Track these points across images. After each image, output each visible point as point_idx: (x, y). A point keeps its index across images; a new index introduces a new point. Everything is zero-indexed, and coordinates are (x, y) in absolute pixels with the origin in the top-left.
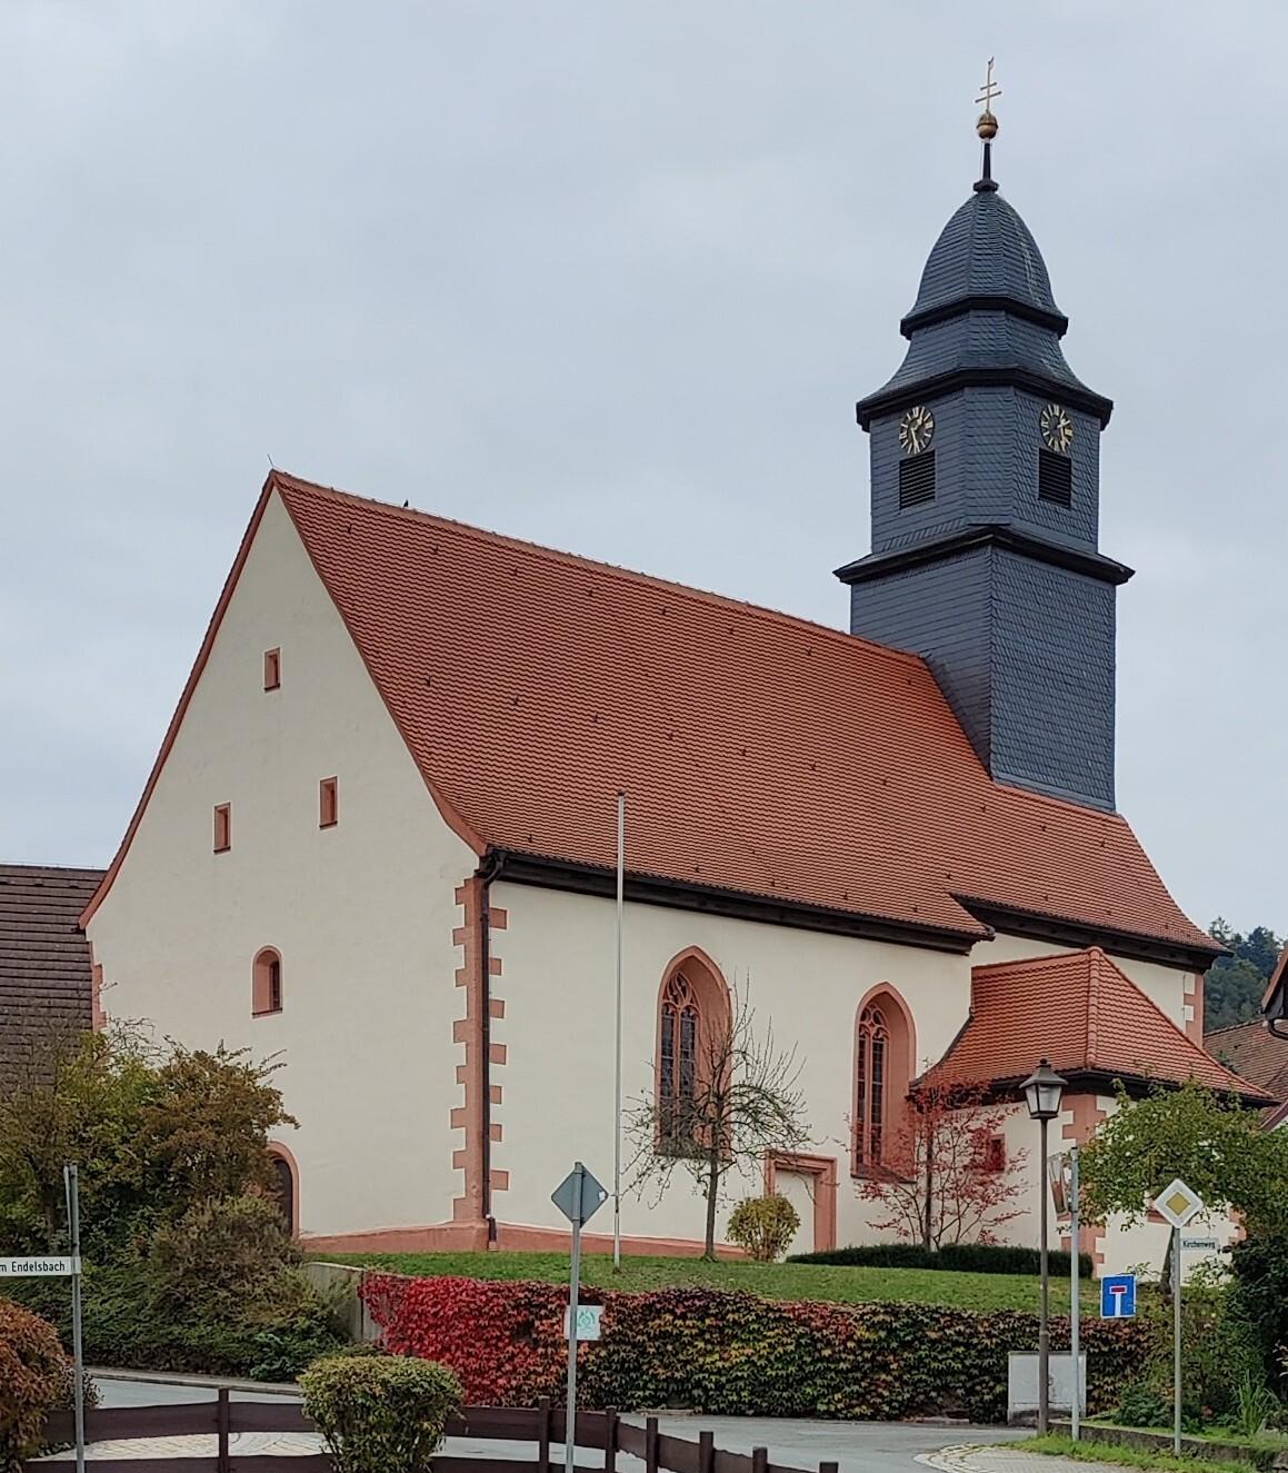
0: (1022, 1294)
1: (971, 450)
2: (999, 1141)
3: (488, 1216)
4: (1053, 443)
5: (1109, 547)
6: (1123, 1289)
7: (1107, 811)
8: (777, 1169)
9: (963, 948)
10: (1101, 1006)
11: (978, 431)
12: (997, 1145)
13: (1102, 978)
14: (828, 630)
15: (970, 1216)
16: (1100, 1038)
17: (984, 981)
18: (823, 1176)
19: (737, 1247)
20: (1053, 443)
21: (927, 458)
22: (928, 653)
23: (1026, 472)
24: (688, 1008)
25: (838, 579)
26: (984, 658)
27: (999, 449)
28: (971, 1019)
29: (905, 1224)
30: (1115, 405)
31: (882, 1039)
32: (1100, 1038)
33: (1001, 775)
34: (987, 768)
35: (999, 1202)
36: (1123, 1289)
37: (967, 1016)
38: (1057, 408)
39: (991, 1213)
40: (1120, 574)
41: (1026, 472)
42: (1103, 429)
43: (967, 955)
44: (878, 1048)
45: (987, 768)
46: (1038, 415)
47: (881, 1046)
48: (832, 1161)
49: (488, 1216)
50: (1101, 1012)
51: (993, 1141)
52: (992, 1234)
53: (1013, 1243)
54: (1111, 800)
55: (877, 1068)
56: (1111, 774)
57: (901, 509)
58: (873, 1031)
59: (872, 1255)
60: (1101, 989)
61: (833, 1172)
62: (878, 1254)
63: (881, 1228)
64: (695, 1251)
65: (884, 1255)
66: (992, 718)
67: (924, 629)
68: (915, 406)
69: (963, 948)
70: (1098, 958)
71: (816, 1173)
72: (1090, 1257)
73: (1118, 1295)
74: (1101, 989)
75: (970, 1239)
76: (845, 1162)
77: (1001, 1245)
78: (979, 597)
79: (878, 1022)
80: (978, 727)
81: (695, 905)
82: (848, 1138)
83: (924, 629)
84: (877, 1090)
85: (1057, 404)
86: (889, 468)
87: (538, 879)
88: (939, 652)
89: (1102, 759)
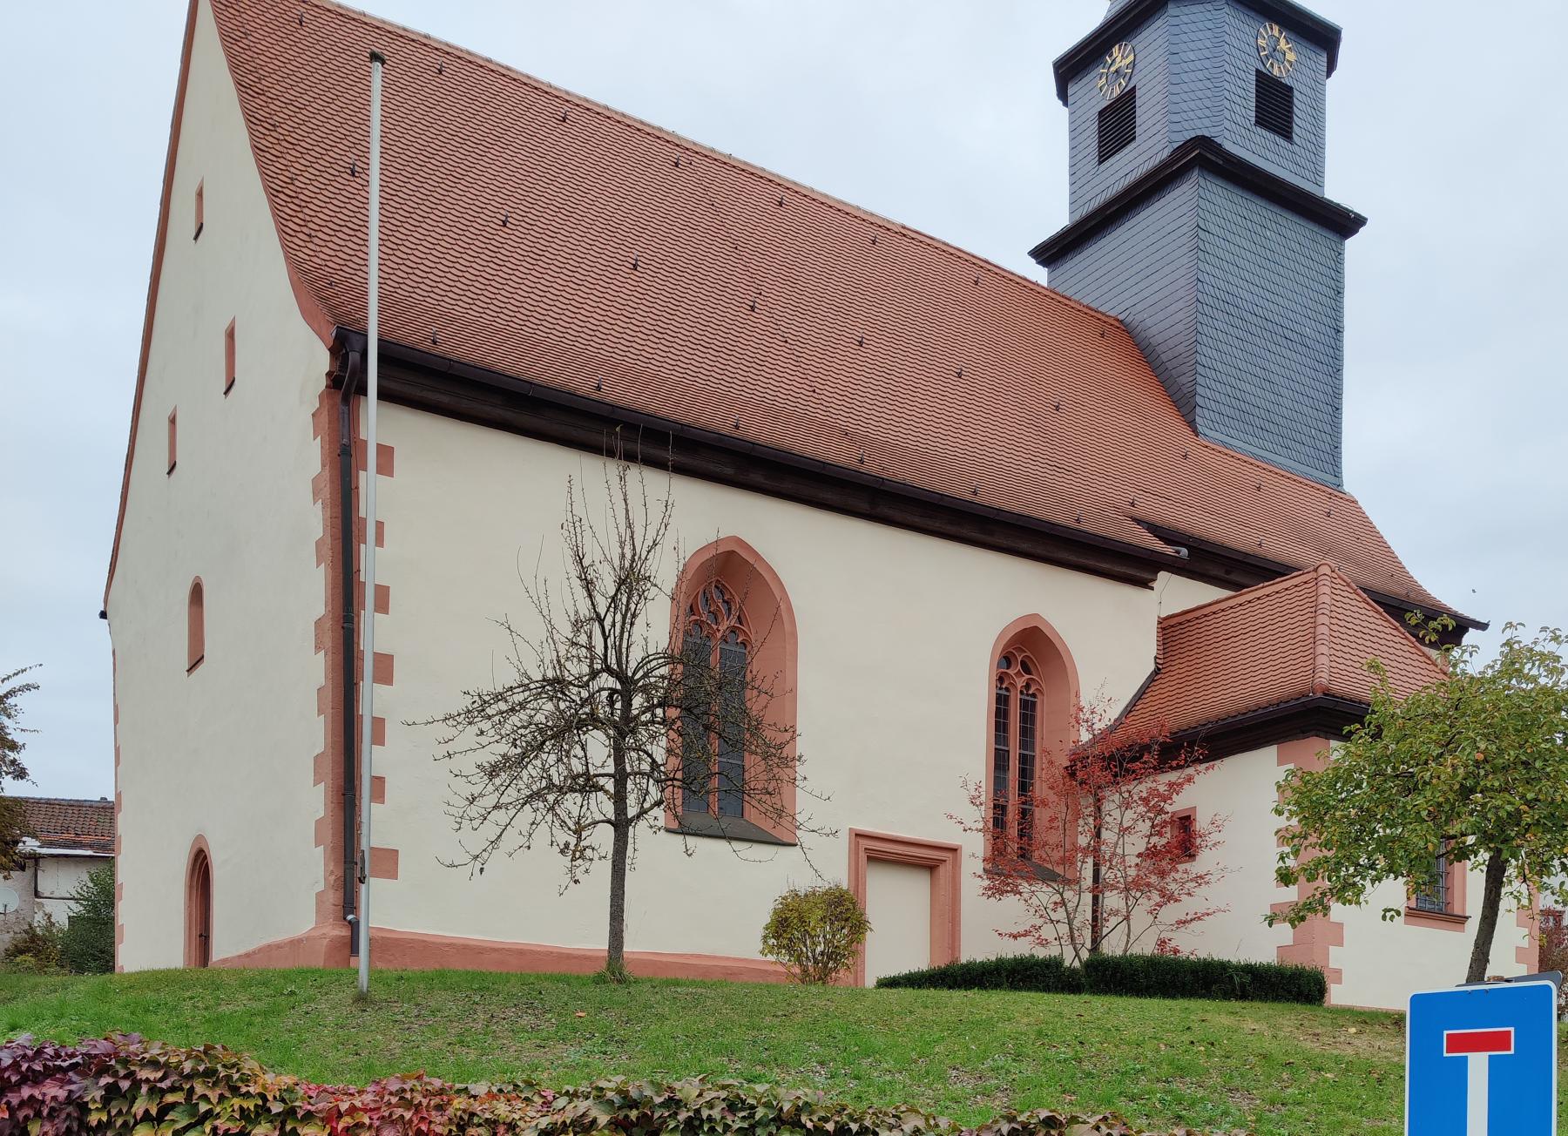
0: (1186, 1037)
1: (1176, 69)
2: (1188, 817)
3: (350, 917)
4: (1272, 64)
5: (1336, 191)
6: (1500, 1041)
7: (1335, 487)
8: (869, 858)
9: (1146, 576)
10: (1335, 628)
11: (1183, 47)
12: (1185, 822)
13: (1334, 597)
14: (1009, 272)
15: (1140, 917)
16: (1334, 664)
17: (1172, 631)
18: (943, 871)
19: (775, 963)
20: (1272, 64)
21: (1128, 98)
22: (1128, 312)
23: (1240, 92)
24: (733, 630)
25: (1034, 261)
26: (1188, 298)
27: (1207, 63)
28: (1157, 671)
29: (1048, 932)
30: (1344, 35)
31: (1034, 695)
32: (1334, 664)
33: (1207, 432)
34: (1192, 425)
35: (1184, 897)
36: (1500, 1041)
37: (1152, 667)
38: (1276, 28)
39: (1170, 913)
40: (1343, 223)
41: (1240, 92)
42: (1329, 74)
43: (1152, 589)
44: (1028, 708)
45: (1192, 425)
46: (1254, 32)
47: (1034, 704)
48: (954, 850)
49: (350, 917)
50: (1334, 634)
51: (1181, 819)
52: (1173, 944)
53: (1203, 953)
54: (1337, 474)
55: (1027, 733)
56: (1336, 447)
57: (1099, 164)
58: (1020, 682)
59: (983, 974)
60: (1333, 608)
61: (956, 865)
62: (991, 973)
63: (1015, 937)
64: (584, 958)
65: (999, 974)
66: (1198, 377)
67: (1123, 287)
68: (1113, 46)
69: (1146, 576)
70: (1328, 572)
71: (931, 867)
72: (1321, 974)
73: (1478, 1064)
74: (1333, 608)
75: (1145, 947)
76: (974, 847)
77: (1183, 955)
78: (1185, 229)
79: (1029, 673)
80: (1183, 380)
81: (729, 471)
82: (978, 816)
83: (1123, 287)
84: (1026, 762)
85: (1277, 23)
86: (1088, 124)
87: (444, 399)
88: (1139, 307)
89: (1327, 428)
